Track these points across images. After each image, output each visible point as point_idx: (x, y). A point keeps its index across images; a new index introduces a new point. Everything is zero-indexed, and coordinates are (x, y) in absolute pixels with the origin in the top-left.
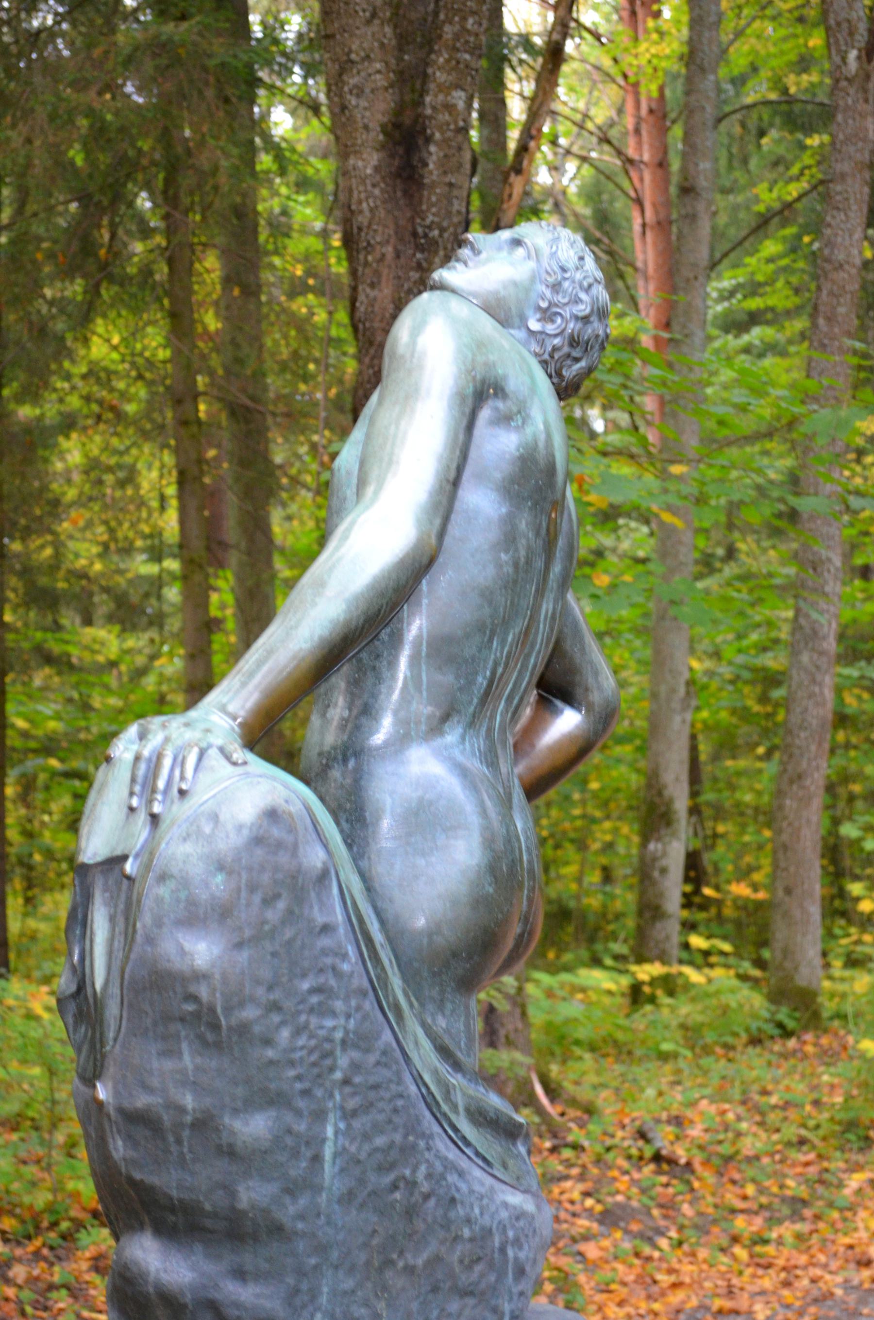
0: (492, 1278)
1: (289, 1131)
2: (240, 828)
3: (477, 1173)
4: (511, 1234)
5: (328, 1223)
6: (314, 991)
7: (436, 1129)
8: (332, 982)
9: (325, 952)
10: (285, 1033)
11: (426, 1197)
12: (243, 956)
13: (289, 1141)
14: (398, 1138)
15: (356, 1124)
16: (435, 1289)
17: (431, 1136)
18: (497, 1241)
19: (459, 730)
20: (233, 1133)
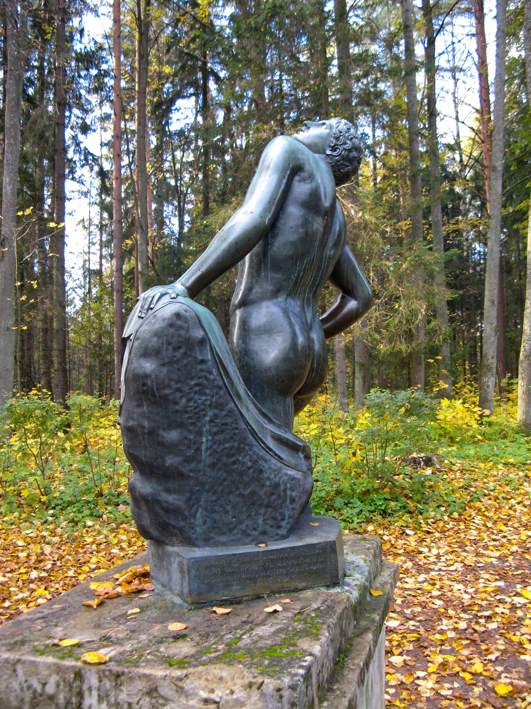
0: (280, 502)
1: (186, 438)
2: (164, 320)
3: (274, 461)
4: (288, 486)
5: (204, 474)
6: (196, 385)
7: (255, 443)
8: (205, 382)
9: (201, 370)
10: (184, 400)
11: (249, 468)
12: (165, 370)
13: (186, 442)
14: (236, 444)
15: (217, 438)
16: (253, 504)
17: (252, 445)
18: (282, 488)
19: (284, 296)
20: (163, 437)
